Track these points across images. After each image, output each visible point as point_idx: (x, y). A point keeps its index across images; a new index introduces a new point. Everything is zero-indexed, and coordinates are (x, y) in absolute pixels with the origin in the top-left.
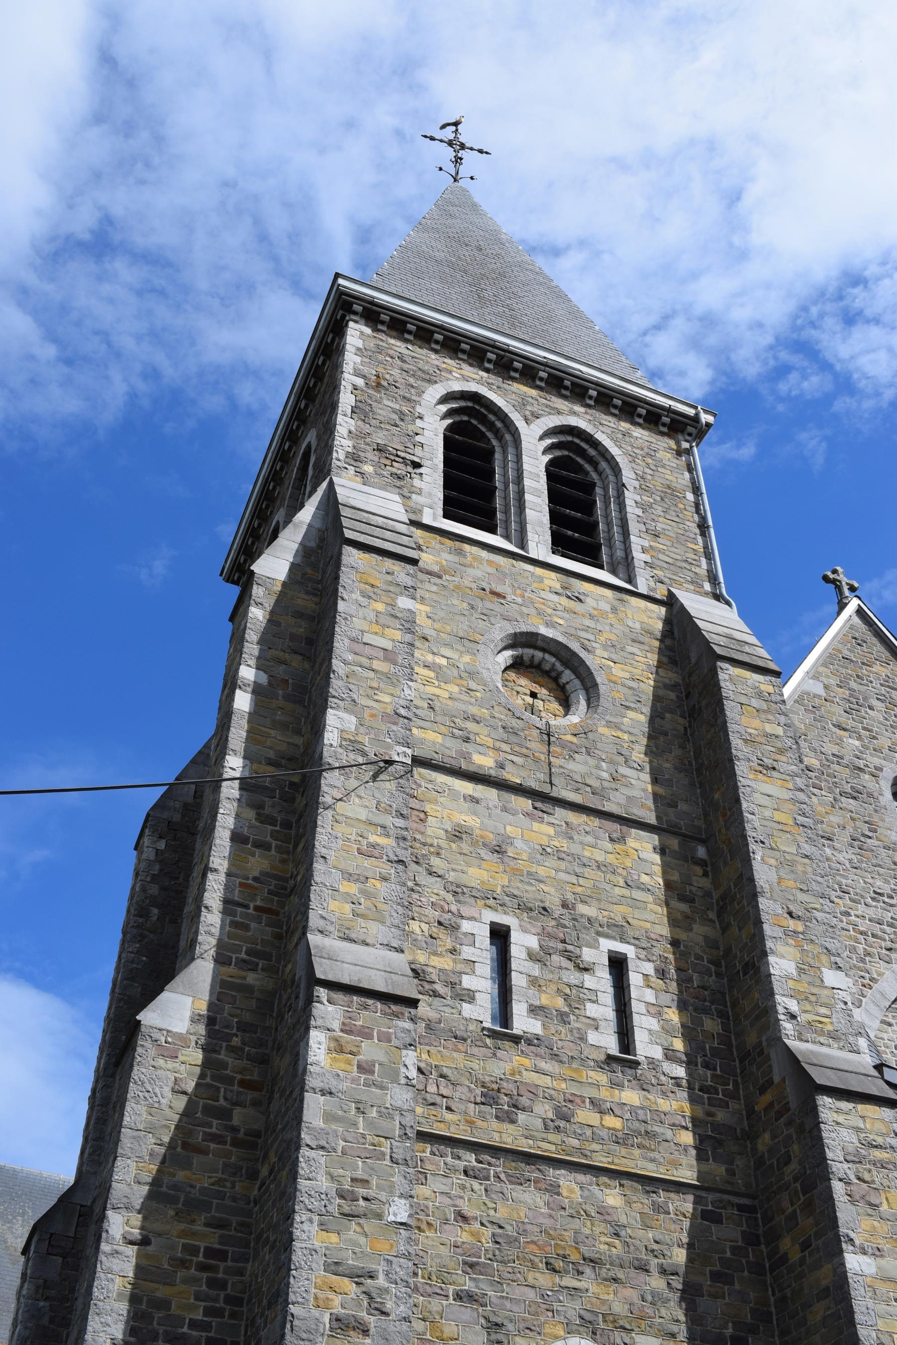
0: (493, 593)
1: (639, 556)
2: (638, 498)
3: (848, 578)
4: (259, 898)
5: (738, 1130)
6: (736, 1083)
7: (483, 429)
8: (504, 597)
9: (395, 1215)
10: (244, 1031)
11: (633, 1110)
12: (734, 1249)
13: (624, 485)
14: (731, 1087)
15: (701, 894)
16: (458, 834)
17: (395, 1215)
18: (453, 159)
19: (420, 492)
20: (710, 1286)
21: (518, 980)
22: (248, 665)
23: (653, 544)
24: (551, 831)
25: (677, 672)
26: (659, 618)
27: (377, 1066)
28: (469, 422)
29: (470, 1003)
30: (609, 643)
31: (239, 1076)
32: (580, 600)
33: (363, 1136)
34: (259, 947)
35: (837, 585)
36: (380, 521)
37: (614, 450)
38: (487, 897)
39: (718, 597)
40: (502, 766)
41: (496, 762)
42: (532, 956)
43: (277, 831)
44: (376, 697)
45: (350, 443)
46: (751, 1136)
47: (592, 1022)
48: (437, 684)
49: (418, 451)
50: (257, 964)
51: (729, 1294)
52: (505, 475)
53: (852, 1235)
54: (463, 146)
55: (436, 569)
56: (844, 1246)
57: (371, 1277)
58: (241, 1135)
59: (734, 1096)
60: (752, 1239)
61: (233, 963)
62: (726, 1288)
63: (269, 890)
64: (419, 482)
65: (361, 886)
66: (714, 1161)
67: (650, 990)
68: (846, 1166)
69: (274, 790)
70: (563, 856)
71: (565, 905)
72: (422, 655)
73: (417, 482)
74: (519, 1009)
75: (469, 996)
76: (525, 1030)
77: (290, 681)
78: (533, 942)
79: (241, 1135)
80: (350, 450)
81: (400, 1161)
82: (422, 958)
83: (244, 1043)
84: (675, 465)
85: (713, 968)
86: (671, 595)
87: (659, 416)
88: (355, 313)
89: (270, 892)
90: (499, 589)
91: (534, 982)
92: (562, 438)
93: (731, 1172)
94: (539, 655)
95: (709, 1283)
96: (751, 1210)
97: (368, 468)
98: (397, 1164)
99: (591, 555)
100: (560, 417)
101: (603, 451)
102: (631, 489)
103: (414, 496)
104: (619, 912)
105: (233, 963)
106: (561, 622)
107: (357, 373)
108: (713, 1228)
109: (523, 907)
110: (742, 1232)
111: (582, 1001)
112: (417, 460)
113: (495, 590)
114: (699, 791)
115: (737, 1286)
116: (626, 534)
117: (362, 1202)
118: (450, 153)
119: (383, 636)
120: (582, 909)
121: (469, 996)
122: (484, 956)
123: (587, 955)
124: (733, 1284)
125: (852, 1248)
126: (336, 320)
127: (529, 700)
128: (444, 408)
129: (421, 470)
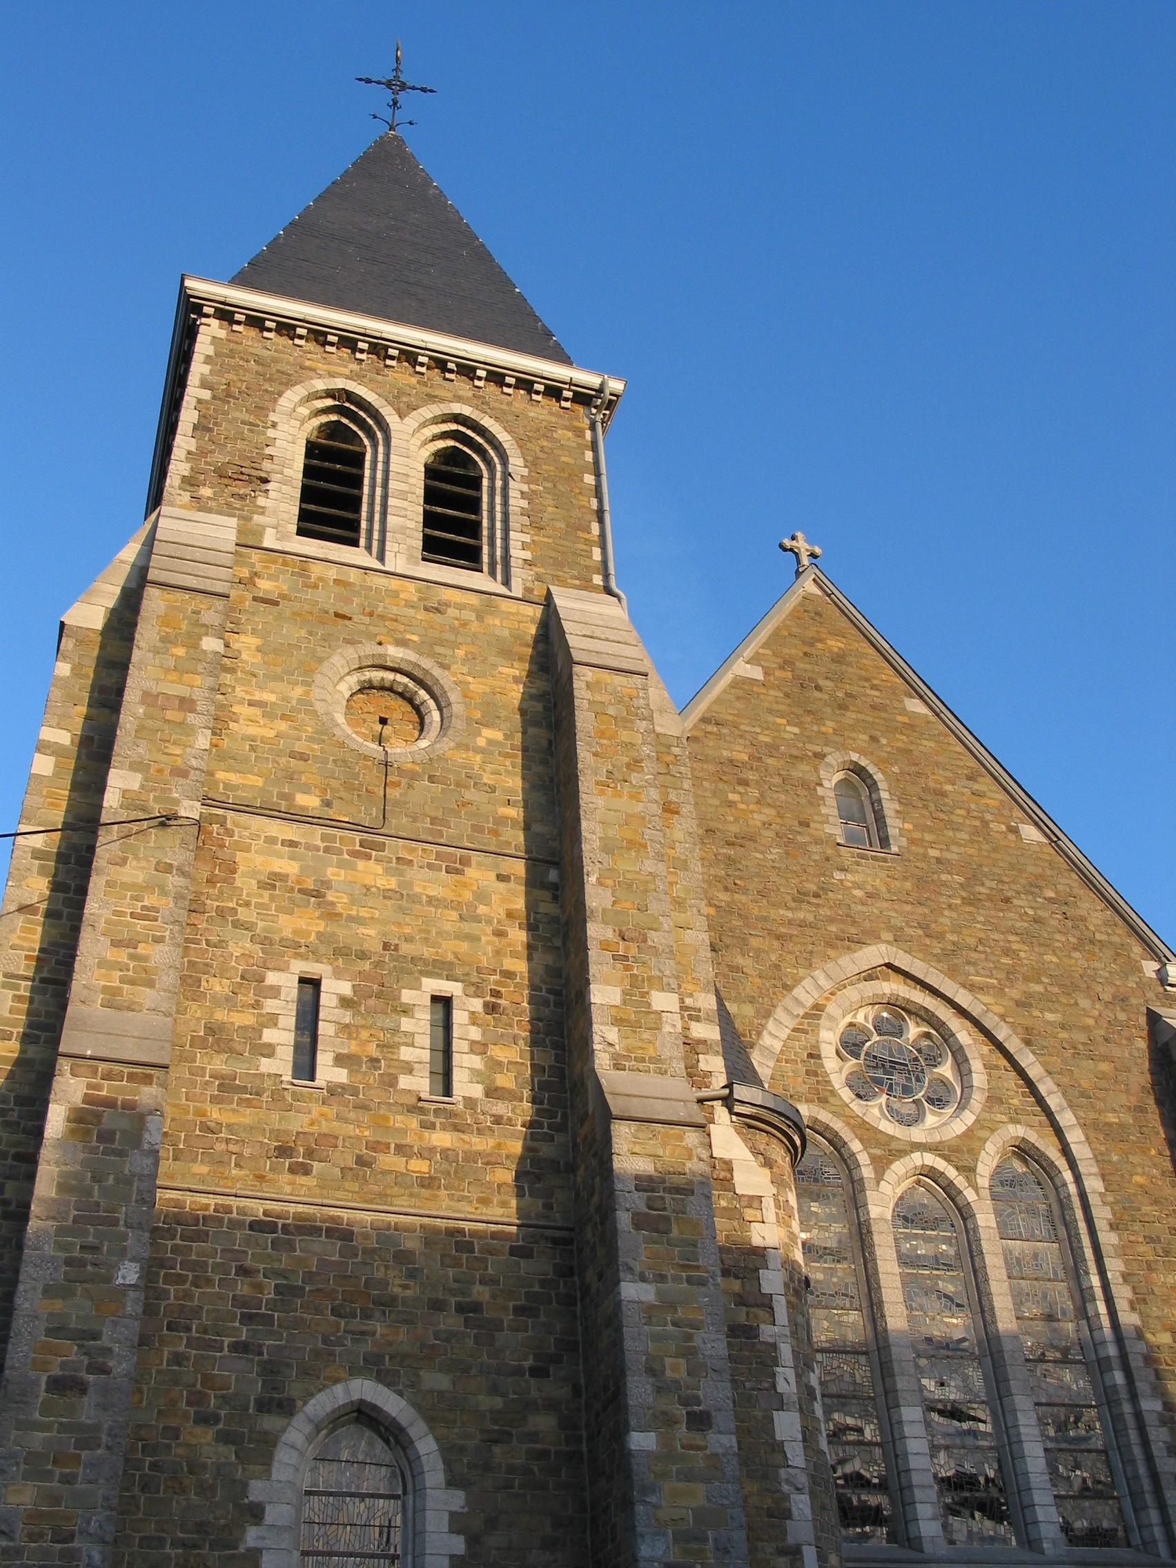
0: (337, 615)
1: (517, 553)
2: (525, 488)
3: (810, 544)
4: (45, 969)
5: (562, 1163)
6: (565, 1115)
7: (355, 428)
8: (350, 619)
9: (124, 1277)
10: (21, 1105)
11: (445, 1152)
12: (543, 1283)
13: (510, 475)
14: (558, 1120)
15: (688, 901)
16: (272, 882)
17: (124, 1277)
18: (391, 103)
19: (262, 511)
20: (512, 1320)
21: (325, 1029)
22: (50, 726)
23: (536, 538)
24: (379, 869)
25: (547, 680)
26: (532, 621)
27: (118, 1133)
28: (338, 422)
29: (269, 1056)
30: (469, 656)
31: (13, 1151)
32: (440, 612)
33: (98, 1204)
34: (42, 1019)
35: (795, 552)
36: (198, 554)
37: (503, 437)
38: (296, 947)
39: (608, 591)
40: (328, 804)
41: (322, 800)
42: (345, 1002)
43: (69, 899)
44: (166, 751)
45: (188, 466)
46: (571, 1169)
47: (406, 1066)
48: (262, 723)
49: (266, 465)
50: (39, 1037)
51: (533, 1327)
52: (373, 478)
53: (632, 1263)
54: (403, 87)
55: (274, 597)
56: (622, 1275)
57: (94, 1339)
58: (13, 1207)
59: (561, 1128)
60: (566, 1272)
61: (14, 1038)
62: (530, 1321)
63: (56, 960)
64: (264, 499)
65: (132, 951)
66: (530, 1196)
67: (475, 1028)
68: (636, 1195)
69: (70, 856)
70: (390, 894)
71: (386, 946)
72: (246, 692)
73: (261, 501)
74: (324, 1059)
75: (269, 1051)
76: (329, 1079)
77: (96, 737)
78: (346, 988)
79: (13, 1207)
80: (186, 473)
81: (135, 1225)
82: (221, 1015)
83: (20, 1117)
84: (575, 445)
85: (552, 998)
86: (549, 596)
87: (560, 390)
88: (207, 316)
89: (58, 963)
90: (345, 610)
91: (345, 1029)
92: (454, 427)
93: (548, 1206)
94: (390, 676)
95: (511, 1317)
96: (568, 1242)
97: (206, 492)
98: (131, 1228)
99: (469, 556)
100: (442, 406)
101: (491, 438)
102: (518, 478)
103: (256, 517)
104: (448, 948)
105: (14, 1038)
106: (415, 638)
107: (204, 385)
108: (523, 1262)
109: (341, 952)
110: (555, 1265)
111: (397, 1046)
112: (264, 475)
113: (340, 612)
114: (557, 809)
115: (543, 1319)
116: (506, 530)
117: (89, 1268)
118: (388, 95)
119: (180, 682)
120: (405, 948)
121: (269, 1051)
122: (290, 1007)
123: (407, 996)
124: (538, 1316)
125: (631, 1276)
126: (189, 326)
127: (379, 727)
128: (304, 411)
129: (269, 486)
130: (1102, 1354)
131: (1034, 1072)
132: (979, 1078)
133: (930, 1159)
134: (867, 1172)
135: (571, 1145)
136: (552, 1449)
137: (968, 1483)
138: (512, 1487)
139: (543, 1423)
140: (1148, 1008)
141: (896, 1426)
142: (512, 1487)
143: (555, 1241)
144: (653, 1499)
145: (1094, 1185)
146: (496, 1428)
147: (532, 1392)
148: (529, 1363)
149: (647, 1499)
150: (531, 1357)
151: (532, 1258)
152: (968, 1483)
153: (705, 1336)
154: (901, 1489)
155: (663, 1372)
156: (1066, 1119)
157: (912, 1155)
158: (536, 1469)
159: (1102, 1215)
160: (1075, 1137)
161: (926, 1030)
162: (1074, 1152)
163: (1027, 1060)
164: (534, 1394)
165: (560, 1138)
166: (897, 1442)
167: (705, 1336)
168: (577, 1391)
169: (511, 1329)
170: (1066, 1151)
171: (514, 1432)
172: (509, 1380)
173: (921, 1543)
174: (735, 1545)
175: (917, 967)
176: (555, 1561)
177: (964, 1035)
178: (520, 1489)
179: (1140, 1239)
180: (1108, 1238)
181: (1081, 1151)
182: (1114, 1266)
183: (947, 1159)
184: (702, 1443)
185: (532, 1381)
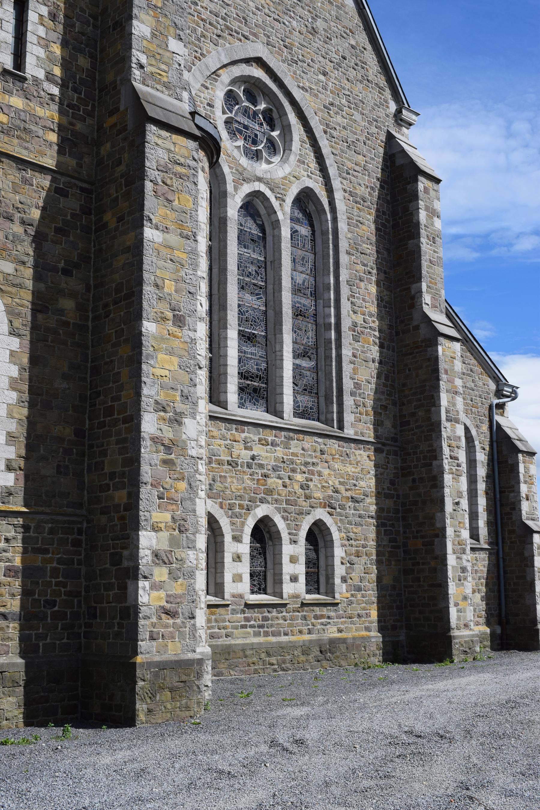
6: (93, 106)
11: (17, 111)
12: (72, 215)
53: (152, 217)
56: (145, 222)
59: (90, 114)
60: (86, 211)
62: (64, 238)
68: (157, 173)
93: (80, 165)
110: (80, 205)
115: (71, 238)
125: (150, 224)
130: (327, 321)
131: (326, 151)
132: (296, 145)
133: (263, 188)
134: (230, 188)
135: (96, 127)
136: (72, 321)
137: (251, 377)
138: (47, 341)
139: (68, 304)
140: (388, 131)
141: (222, 340)
142: (47, 341)
143: (82, 189)
144: (152, 362)
145: (342, 226)
146: (40, 303)
147: (62, 284)
148: (62, 265)
149: (149, 362)
150: (63, 261)
151: (68, 197)
152: (251, 377)
153: (187, 271)
154: (220, 375)
155: (163, 288)
156: (336, 184)
157: (255, 183)
158: (61, 332)
159: (343, 245)
160: (338, 195)
161: (271, 107)
162: (337, 204)
163: (324, 143)
164: (63, 285)
165: (89, 120)
166: (222, 349)
167: (187, 271)
168: (88, 288)
169: (52, 241)
170: (332, 203)
171: (50, 307)
172: (49, 274)
173: (227, 404)
174: (191, 395)
175: (272, 63)
176: (69, 388)
177: (292, 117)
178: (51, 343)
179: (359, 262)
180: (344, 259)
181: (340, 206)
182: (344, 276)
183: (272, 190)
184: (180, 335)
185: (63, 277)
